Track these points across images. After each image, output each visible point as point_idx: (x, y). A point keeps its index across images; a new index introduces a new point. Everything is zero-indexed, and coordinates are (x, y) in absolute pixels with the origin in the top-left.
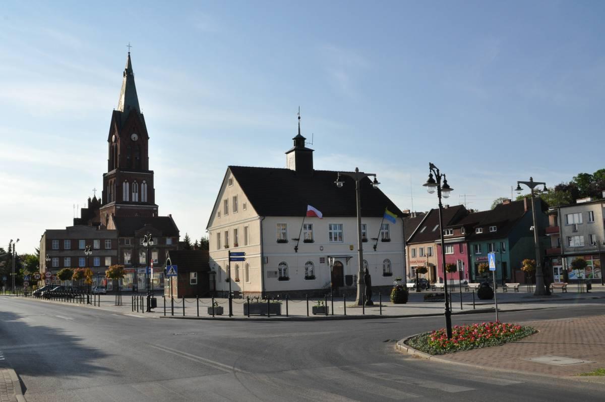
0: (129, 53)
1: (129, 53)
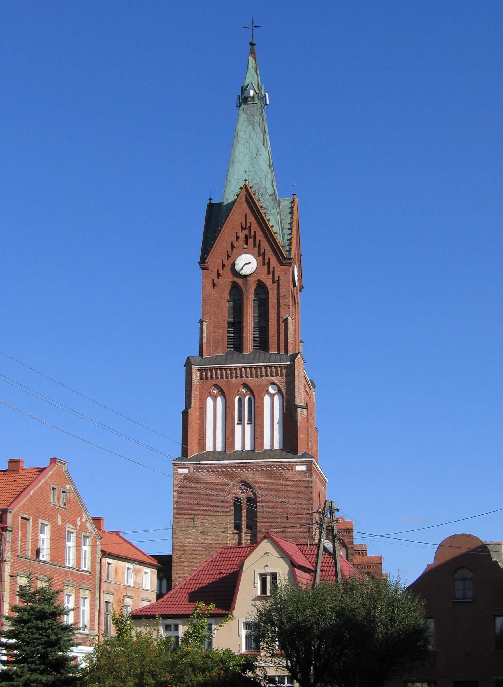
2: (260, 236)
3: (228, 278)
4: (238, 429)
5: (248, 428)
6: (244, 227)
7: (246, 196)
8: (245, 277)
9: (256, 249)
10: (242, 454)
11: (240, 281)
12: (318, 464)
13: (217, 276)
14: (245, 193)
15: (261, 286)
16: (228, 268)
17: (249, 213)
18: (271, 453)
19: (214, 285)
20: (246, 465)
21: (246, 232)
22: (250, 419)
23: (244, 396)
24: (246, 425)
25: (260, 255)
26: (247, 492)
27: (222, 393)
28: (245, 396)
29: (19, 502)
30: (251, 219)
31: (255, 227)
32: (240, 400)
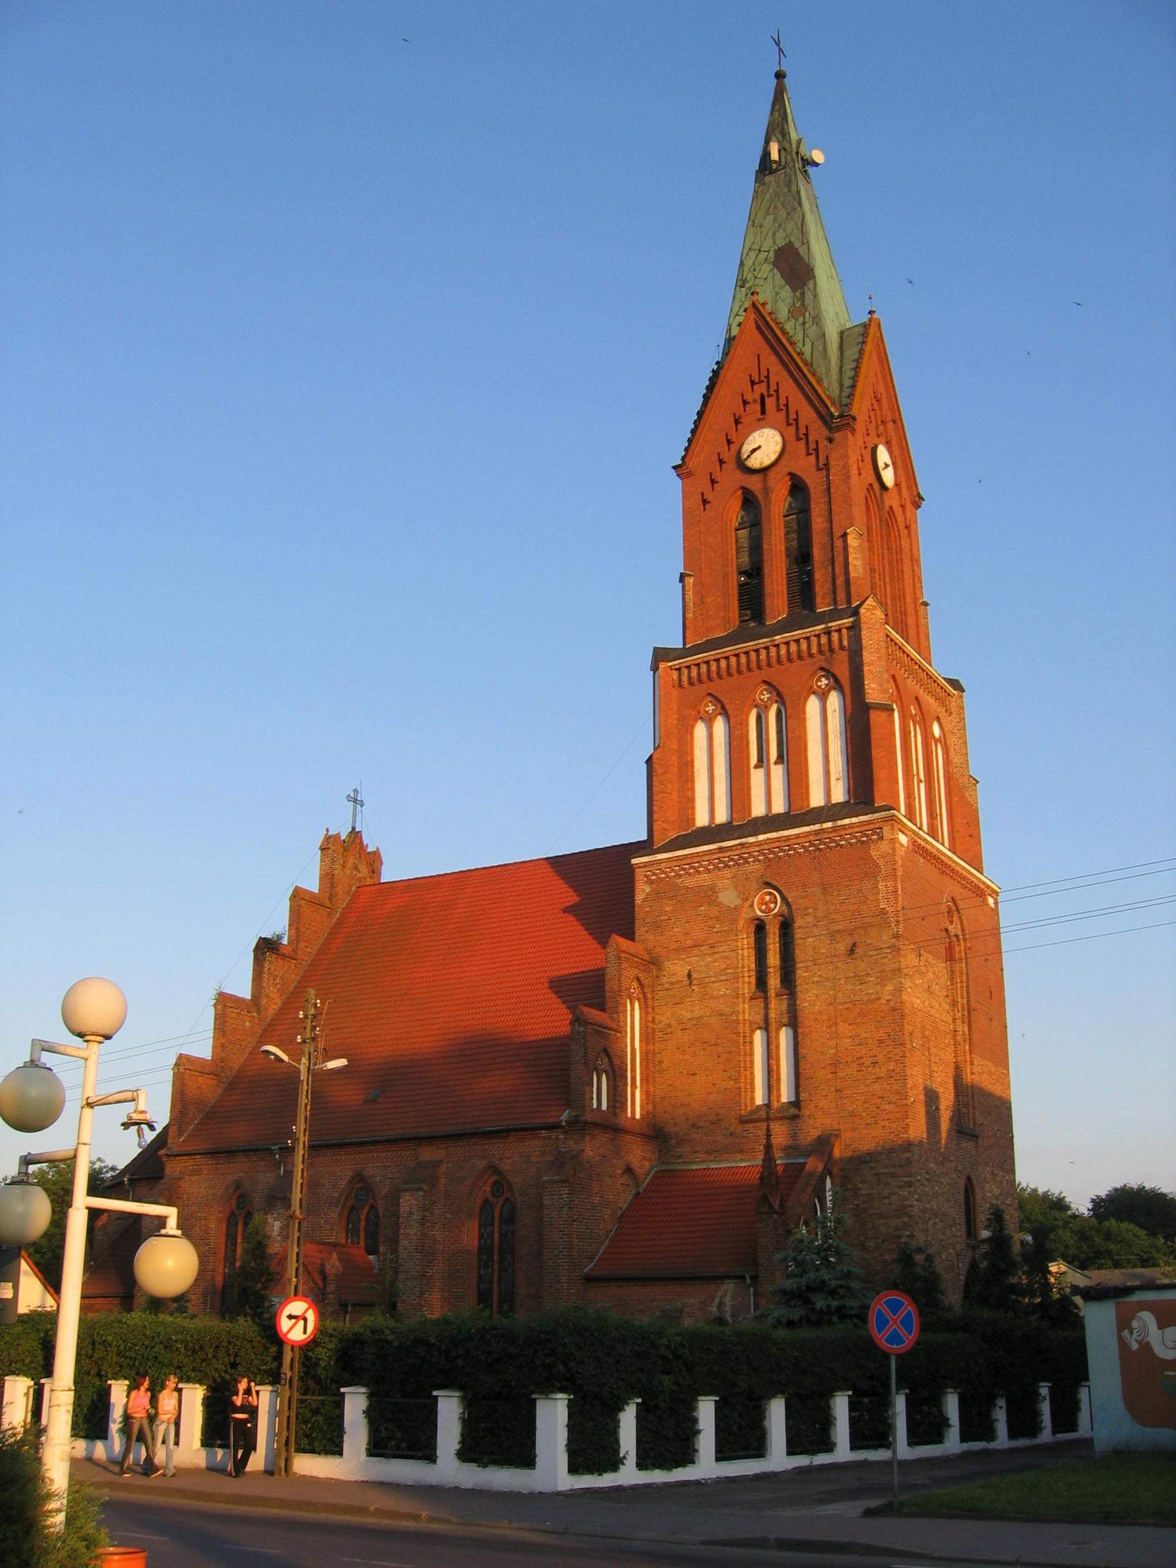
0: (780, 76)
1: (780, 76)
2: (788, 388)
3: (731, 479)
4: (757, 777)
5: (778, 772)
6: (757, 381)
7: (756, 323)
8: (764, 471)
9: (783, 414)
10: (771, 822)
11: (754, 483)
12: (931, 666)
13: (750, 384)
14: (753, 316)
15: (798, 487)
16: (731, 465)
17: (766, 351)
18: (831, 812)
19: (705, 502)
20: (748, 1077)
21: (761, 389)
22: (780, 759)
23: (766, 707)
24: (773, 767)
25: (791, 425)
26: (776, 907)
27: (725, 712)
28: (767, 708)
29: (300, 1119)
30: (770, 361)
31: (778, 374)
32: (759, 719)
